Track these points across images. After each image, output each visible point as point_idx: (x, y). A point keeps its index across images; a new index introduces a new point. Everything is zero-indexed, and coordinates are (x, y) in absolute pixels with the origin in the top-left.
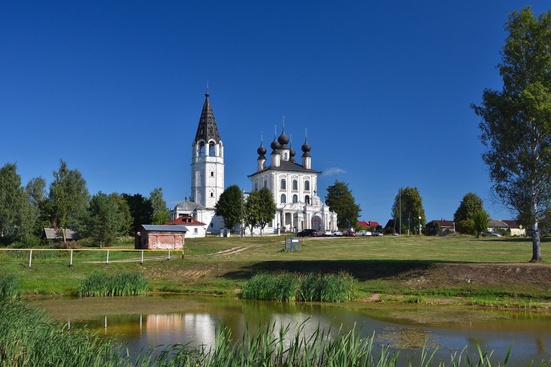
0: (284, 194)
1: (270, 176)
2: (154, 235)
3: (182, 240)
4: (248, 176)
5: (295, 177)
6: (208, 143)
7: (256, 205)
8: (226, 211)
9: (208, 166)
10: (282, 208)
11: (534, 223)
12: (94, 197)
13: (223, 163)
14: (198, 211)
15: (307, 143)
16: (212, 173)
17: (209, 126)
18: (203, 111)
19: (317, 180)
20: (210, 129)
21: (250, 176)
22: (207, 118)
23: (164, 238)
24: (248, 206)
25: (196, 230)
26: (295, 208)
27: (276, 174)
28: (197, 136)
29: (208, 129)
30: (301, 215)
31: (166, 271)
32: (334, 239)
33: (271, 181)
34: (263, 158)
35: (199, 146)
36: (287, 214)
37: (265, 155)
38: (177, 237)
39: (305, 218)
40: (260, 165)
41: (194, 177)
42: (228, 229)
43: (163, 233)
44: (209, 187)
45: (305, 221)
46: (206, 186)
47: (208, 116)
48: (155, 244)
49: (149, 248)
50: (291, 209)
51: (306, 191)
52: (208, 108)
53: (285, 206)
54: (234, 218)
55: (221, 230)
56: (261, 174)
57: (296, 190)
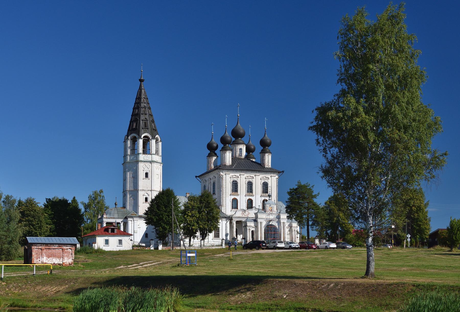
0: (236, 198)
1: (218, 177)
2: (39, 249)
3: (72, 254)
4: (196, 177)
5: (251, 177)
6: (142, 139)
7: (193, 212)
8: (156, 219)
9: (141, 166)
10: (232, 215)
11: (368, 237)
12: (20, 202)
13: (161, 162)
14: (129, 219)
15: (266, 136)
16: (147, 175)
17: (142, 117)
18: (136, 99)
19: (278, 182)
20: (144, 121)
21: (199, 177)
22: (141, 109)
23: (50, 251)
24: (184, 212)
25: (120, 242)
26: (248, 214)
27: (225, 174)
28: (129, 130)
29: (141, 122)
30: (251, 224)
31: (26, 286)
32: (283, 252)
33: (219, 183)
34: (214, 155)
35: (130, 143)
36: (237, 222)
37: (216, 152)
38: (66, 250)
39: (256, 227)
40: (210, 163)
41: (125, 180)
42: (160, 240)
43: (49, 246)
44: (143, 190)
45: (257, 231)
46: (140, 189)
47: (142, 105)
48: (39, 258)
49: (32, 263)
50: (244, 216)
51: (264, 194)
52: (143, 96)
53: (235, 213)
54: (166, 227)
55: (151, 241)
56: (209, 174)
57: (251, 194)
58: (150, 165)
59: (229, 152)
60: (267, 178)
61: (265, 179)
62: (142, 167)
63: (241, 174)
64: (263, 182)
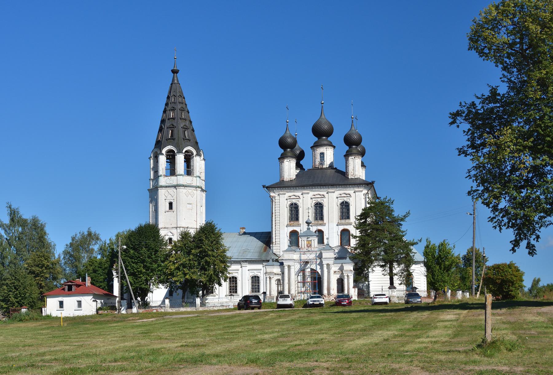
9: (162, 193)
16: (171, 204)
27: (279, 195)
44: (165, 228)
51: (343, 221)
57: (320, 222)
58: (175, 190)
59: (289, 160)
60: (348, 195)
61: (344, 197)
62: (163, 195)
63: (304, 192)
64: (340, 201)
